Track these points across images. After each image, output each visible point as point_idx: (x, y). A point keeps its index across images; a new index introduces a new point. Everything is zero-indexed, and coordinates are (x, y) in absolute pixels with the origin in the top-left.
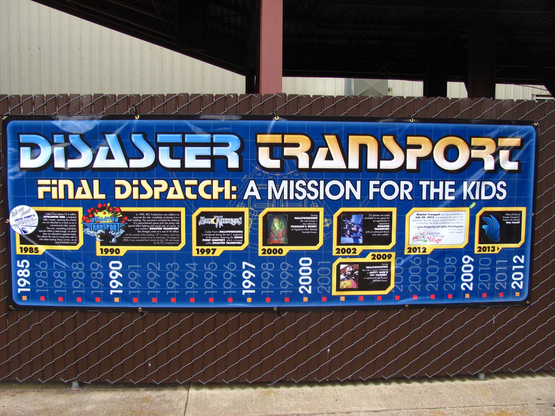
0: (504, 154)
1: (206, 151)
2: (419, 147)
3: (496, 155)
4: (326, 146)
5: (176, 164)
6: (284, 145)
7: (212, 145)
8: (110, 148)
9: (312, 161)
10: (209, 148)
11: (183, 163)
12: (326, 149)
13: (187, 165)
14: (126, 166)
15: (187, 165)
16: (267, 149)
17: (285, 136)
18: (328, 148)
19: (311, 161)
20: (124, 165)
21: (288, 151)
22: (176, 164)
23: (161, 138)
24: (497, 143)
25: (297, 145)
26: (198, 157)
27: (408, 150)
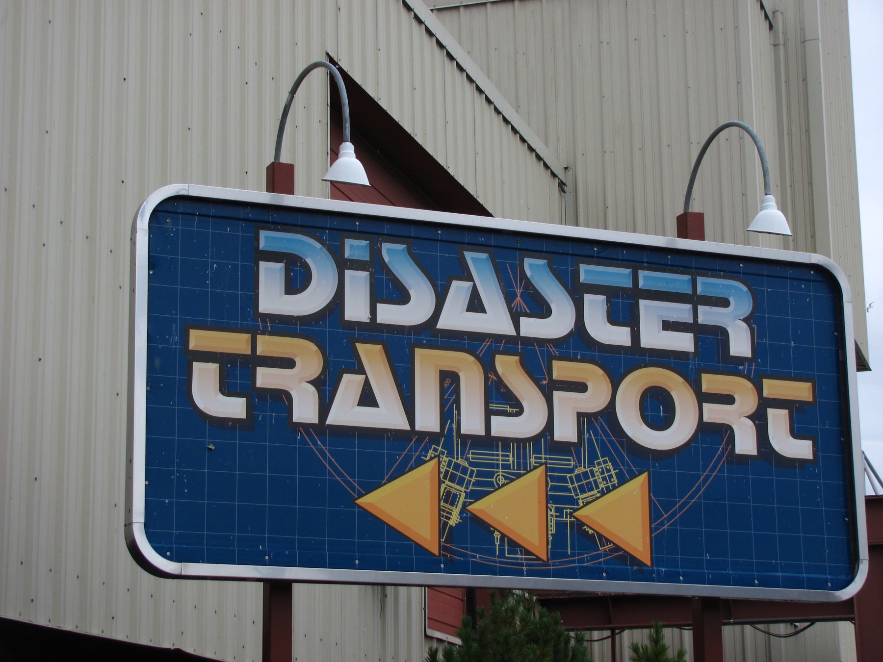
0: (778, 419)
1: (681, 312)
2: (580, 387)
3: (759, 419)
4: (361, 370)
5: (620, 336)
6: (254, 361)
7: (695, 300)
8: (475, 287)
9: (325, 407)
10: (248, 336)
11: (636, 336)
12: (361, 378)
13: (647, 341)
14: (510, 331)
15: (647, 341)
16: (214, 367)
17: (260, 339)
18: (364, 376)
19: (324, 408)
20: (508, 329)
21: (266, 378)
22: (620, 336)
23: (587, 273)
24: (759, 389)
25: (288, 363)
26: (668, 326)
27: (557, 395)
